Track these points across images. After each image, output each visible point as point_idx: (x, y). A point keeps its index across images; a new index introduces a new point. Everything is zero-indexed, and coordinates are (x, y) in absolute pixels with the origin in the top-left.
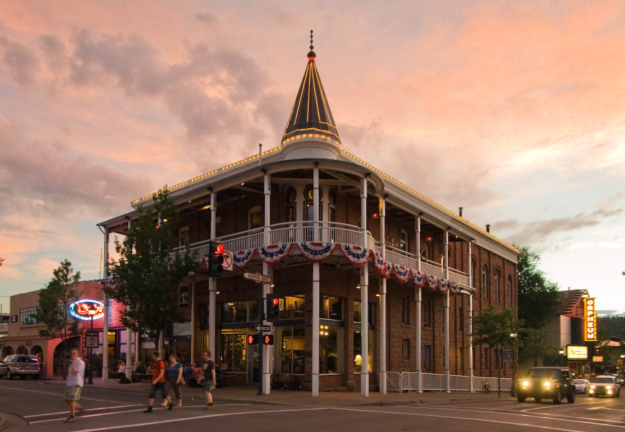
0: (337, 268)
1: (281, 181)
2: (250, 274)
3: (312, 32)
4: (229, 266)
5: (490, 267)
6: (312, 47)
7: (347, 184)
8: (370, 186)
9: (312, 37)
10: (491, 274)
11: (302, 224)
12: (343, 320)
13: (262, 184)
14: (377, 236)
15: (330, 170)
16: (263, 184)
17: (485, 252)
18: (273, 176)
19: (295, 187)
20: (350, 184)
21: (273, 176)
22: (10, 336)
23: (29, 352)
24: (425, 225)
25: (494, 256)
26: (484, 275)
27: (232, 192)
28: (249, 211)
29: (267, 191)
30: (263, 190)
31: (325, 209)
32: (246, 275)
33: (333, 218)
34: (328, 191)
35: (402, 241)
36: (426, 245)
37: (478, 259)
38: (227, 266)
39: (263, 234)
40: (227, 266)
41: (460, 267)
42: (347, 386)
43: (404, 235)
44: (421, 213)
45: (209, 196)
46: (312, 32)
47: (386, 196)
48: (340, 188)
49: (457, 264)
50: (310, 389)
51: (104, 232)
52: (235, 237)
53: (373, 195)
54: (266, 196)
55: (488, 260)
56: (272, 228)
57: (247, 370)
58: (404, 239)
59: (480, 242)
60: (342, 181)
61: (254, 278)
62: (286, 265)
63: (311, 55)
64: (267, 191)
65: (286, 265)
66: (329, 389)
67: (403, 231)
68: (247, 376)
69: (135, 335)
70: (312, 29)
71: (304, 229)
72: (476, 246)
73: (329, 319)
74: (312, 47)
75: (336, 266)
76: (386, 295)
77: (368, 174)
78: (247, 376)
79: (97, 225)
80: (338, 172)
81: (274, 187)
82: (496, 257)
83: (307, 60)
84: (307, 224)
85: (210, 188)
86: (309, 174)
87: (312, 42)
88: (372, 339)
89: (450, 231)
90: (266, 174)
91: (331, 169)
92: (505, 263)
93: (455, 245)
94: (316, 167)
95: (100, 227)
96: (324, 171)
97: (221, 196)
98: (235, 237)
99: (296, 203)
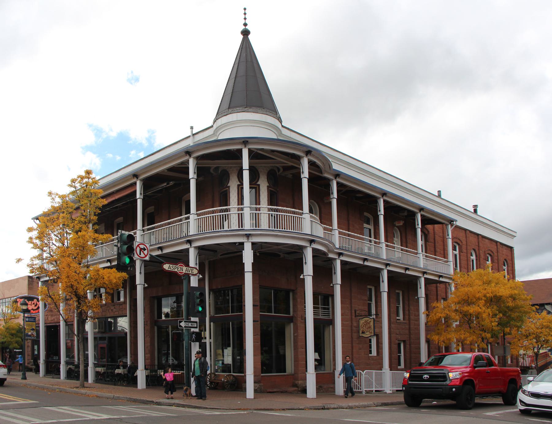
0: (281, 257)
1: (212, 164)
2: (171, 265)
3: (245, 9)
4: (146, 256)
5: (479, 252)
6: (245, 25)
7: (287, 164)
8: (312, 164)
9: (245, 14)
10: (481, 259)
11: (237, 209)
12: (291, 314)
14: (325, 219)
15: (262, 150)
16: (188, 168)
17: (473, 235)
18: (198, 158)
19: (228, 170)
20: (290, 164)
21: (198, 158)
24: (388, 206)
25: (484, 239)
26: (473, 261)
28: (183, 198)
29: (192, 174)
30: (188, 173)
33: (272, 201)
34: (267, 172)
35: (365, 225)
36: (397, 229)
37: (464, 243)
38: (144, 256)
39: (189, 222)
40: (144, 256)
41: (442, 252)
42: (298, 387)
45: (135, 184)
46: (245, 9)
47: (338, 175)
48: (282, 170)
49: (438, 250)
50: (244, 390)
52: (169, 224)
53: (321, 175)
54: (191, 180)
55: (477, 244)
56: (198, 215)
58: (368, 223)
59: (461, 222)
61: (176, 270)
62: (221, 255)
63: (246, 33)
64: (192, 174)
65: (221, 255)
66: (275, 390)
67: (366, 214)
71: (239, 214)
72: (457, 227)
73: (273, 314)
74: (245, 25)
75: (279, 256)
76: (341, 286)
77: (309, 151)
79: (32, 219)
80: (273, 151)
81: (200, 171)
82: (487, 240)
83: (241, 37)
84: (257, 209)
85: (135, 175)
86: (238, 154)
87: (245, 19)
88: (148, 339)
89: (422, 213)
90: (190, 157)
91: (263, 148)
92: (499, 247)
93: (434, 228)
95: (35, 220)
96: (256, 150)
97: (148, 183)
98: (169, 224)
99: (229, 187)
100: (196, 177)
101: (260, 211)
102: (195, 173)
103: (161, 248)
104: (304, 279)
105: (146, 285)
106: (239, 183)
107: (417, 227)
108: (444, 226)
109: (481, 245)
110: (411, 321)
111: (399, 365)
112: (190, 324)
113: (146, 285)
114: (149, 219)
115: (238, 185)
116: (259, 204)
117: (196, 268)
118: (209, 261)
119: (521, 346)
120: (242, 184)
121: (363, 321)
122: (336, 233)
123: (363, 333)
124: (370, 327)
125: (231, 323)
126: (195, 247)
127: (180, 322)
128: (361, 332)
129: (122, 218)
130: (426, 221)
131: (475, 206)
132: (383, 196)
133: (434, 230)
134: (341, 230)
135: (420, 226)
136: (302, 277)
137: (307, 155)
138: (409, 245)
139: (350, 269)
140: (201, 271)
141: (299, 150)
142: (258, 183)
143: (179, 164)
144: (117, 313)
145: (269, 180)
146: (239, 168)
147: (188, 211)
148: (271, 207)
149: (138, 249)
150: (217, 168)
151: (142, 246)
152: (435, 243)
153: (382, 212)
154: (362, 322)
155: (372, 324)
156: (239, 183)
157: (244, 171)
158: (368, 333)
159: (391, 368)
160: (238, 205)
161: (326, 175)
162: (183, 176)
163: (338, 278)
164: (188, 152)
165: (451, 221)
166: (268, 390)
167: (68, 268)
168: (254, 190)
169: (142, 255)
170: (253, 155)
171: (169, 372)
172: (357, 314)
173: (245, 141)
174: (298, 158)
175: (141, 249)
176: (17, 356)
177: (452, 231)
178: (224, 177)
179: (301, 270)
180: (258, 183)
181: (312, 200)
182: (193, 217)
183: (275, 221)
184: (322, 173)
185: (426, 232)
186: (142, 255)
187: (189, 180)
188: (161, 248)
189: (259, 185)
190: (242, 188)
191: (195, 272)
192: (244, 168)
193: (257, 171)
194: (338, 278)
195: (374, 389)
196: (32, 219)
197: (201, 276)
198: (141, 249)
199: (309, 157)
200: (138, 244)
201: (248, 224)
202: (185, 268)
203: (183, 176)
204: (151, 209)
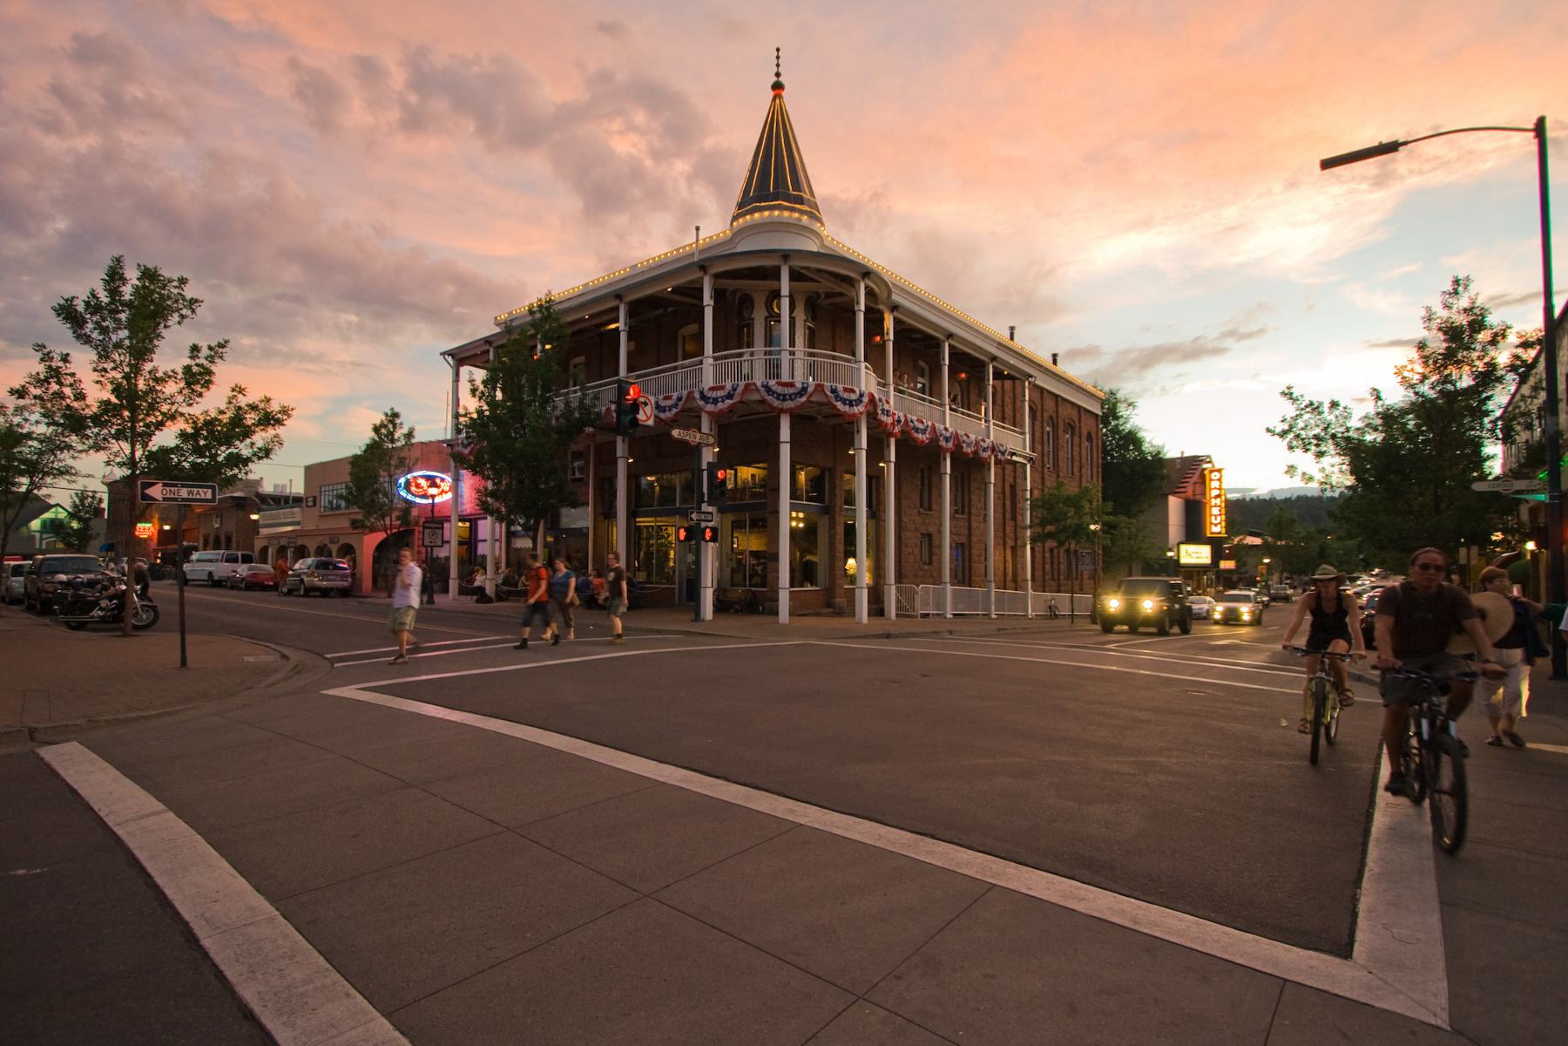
0: (818, 421)
3: (778, 50)
4: (649, 418)
6: (778, 75)
8: (870, 293)
11: (763, 353)
14: (880, 371)
15: (807, 268)
16: (701, 290)
17: (1050, 396)
20: (838, 290)
21: (717, 276)
24: (954, 354)
29: (708, 300)
30: (701, 299)
32: (675, 433)
33: (812, 342)
34: (804, 300)
37: (1039, 407)
43: (923, 370)
44: (950, 336)
46: (778, 50)
48: (823, 296)
49: (1006, 416)
57: (677, 581)
58: (923, 377)
61: (688, 438)
64: (708, 300)
67: (921, 363)
68: (677, 591)
71: (766, 360)
72: (1037, 386)
74: (778, 75)
75: (816, 418)
77: (867, 273)
78: (677, 591)
79: (441, 354)
80: (820, 271)
81: (718, 294)
83: (771, 94)
84: (770, 353)
86: (775, 274)
87: (778, 65)
88: (872, 533)
90: (706, 273)
92: (1082, 414)
93: (1003, 385)
94: (785, 263)
95: (446, 357)
96: (798, 269)
97: (635, 309)
99: (753, 319)
100: (712, 303)
101: (794, 355)
102: (711, 297)
108: (1017, 382)
109: (1060, 410)
110: (972, 517)
116: (794, 347)
117: (712, 436)
125: (106, 517)
127: (692, 513)
129: (584, 357)
131: (1055, 356)
132: (948, 339)
133: (1003, 389)
138: (972, 409)
141: (854, 271)
143: (686, 283)
148: (811, 350)
150: (735, 292)
152: (1003, 406)
160: (766, 346)
166: (799, 612)
174: (850, 282)
179: (851, 443)
183: (812, 370)
187: (703, 307)
196: (441, 354)
199: (791, 264)
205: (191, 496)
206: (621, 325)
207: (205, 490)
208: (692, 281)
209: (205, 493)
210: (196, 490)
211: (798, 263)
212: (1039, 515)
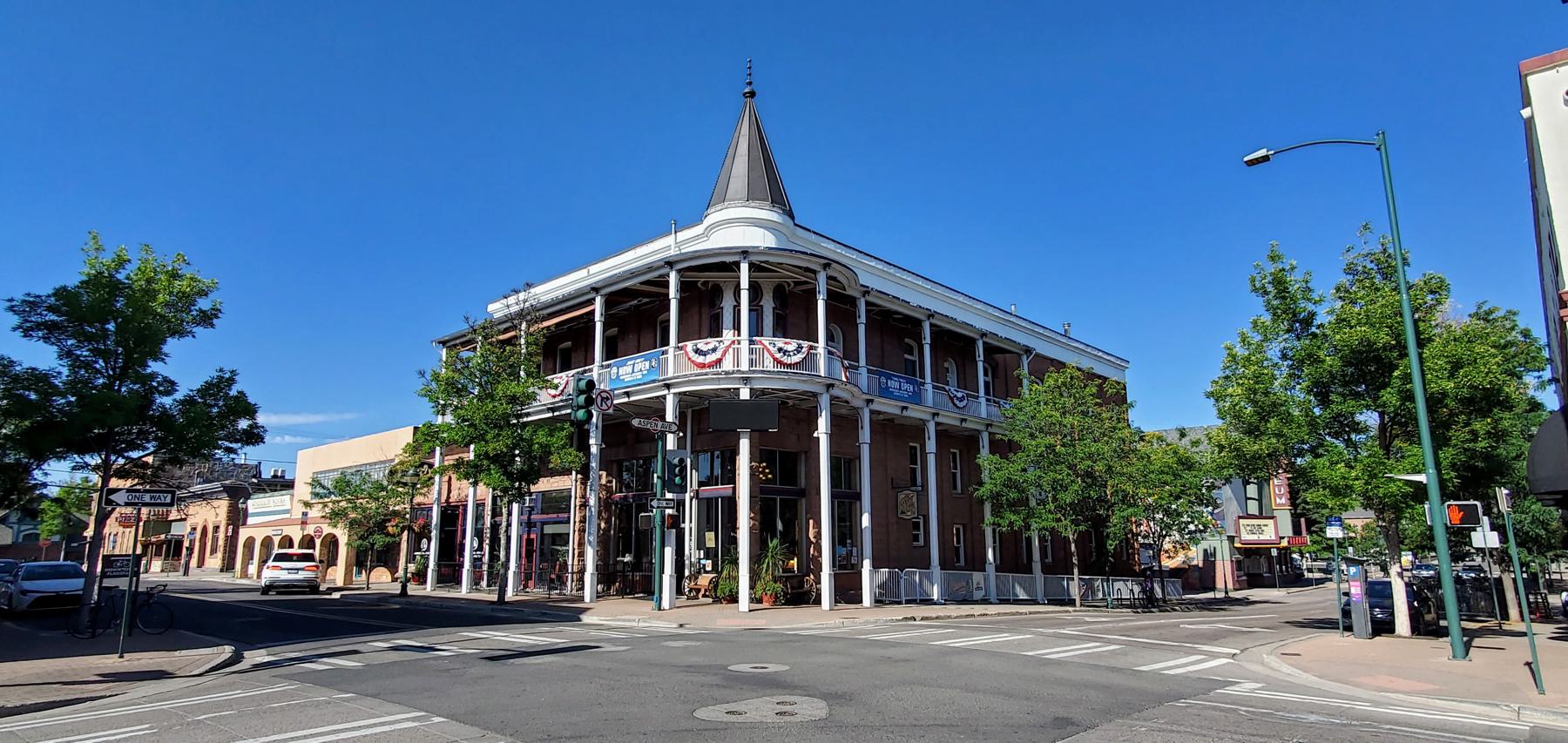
4: (609, 408)
13: (666, 285)
14: (850, 353)
22: (293, 517)
23: (296, 544)
24: (938, 333)
27: (627, 293)
31: (767, 316)
32: (635, 422)
43: (911, 347)
44: (931, 315)
45: (594, 299)
47: (866, 291)
48: (792, 284)
51: (163, 630)
57: (66, 563)
60: (790, 277)
61: (649, 426)
68: (1210, 595)
69: (943, 416)
70: (525, 281)
78: (1210, 595)
81: (684, 287)
90: (672, 268)
94: (745, 258)
97: (611, 301)
103: (628, 394)
104: (818, 438)
105: (604, 446)
106: (735, 304)
107: (977, 359)
111: (958, 561)
112: (665, 502)
113: (604, 446)
114: (611, 352)
115: (735, 307)
118: (693, 411)
119: (1486, 519)
120: (739, 305)
121: (903, 496)
122: (863, 371)
123: (903, 513)
124: (913, 504)
126: (674, 394)
127: (652, 500)
128: (899, 511)
130: (989, 350)
134: (871, 368)
135: (982, 358)
136: (815, 435)
137: (825, 270)
139: (884, 420)
140: (682, 426)
142: (762, 303)
144: (557, 484)
145: (775, 298)
146: (736, 283)
147: (665, 342)
149: (599, 398)
150: (705, 283)
151: (604, 395)
153: (928, 340)
154: (901, 496)
155: (915, 499)
156: (735, 304)
157: (742, 291)
158: (909, 513)
159: (943, 566)
161: (850, 292)
162: (662, 290)
163: (865, 435)
164: (670, 264)
165: (1028, 351)
167: (432, 378)
168: (755, 313)
169: (605, 407)
170: (753, 267)
171: (856, 409)
172: (894, 486)
173: (745, 253)
175: (603, 399)
176: (1462, 513)
177: (1029, 364)
178: (716, 293)
180: (762, 303)
181: (834, 323)
182: (671, 349)
184: (845, 290)
185: (994, 365)
186: (605, 407)
188: (628, 394)
189: (762, 306)
190: (739, 310)
191: (674, 428)
192: (742, 287)
193: (760, 287)
194: (865, 435)
195: (918, 598)
197: (681, 434)
198: (603, 399)
200: (598, 391)
201: (745, 366)
202: (660, 424)
203: (662, 290)
204: (614, 331)
205: (153, 501)
206: (61, 561)
207: (165, 495)
208: (660, 276)
209: (165, 498)
210: (158, 495)
211: (754, 259)
212: (1518, 465)
